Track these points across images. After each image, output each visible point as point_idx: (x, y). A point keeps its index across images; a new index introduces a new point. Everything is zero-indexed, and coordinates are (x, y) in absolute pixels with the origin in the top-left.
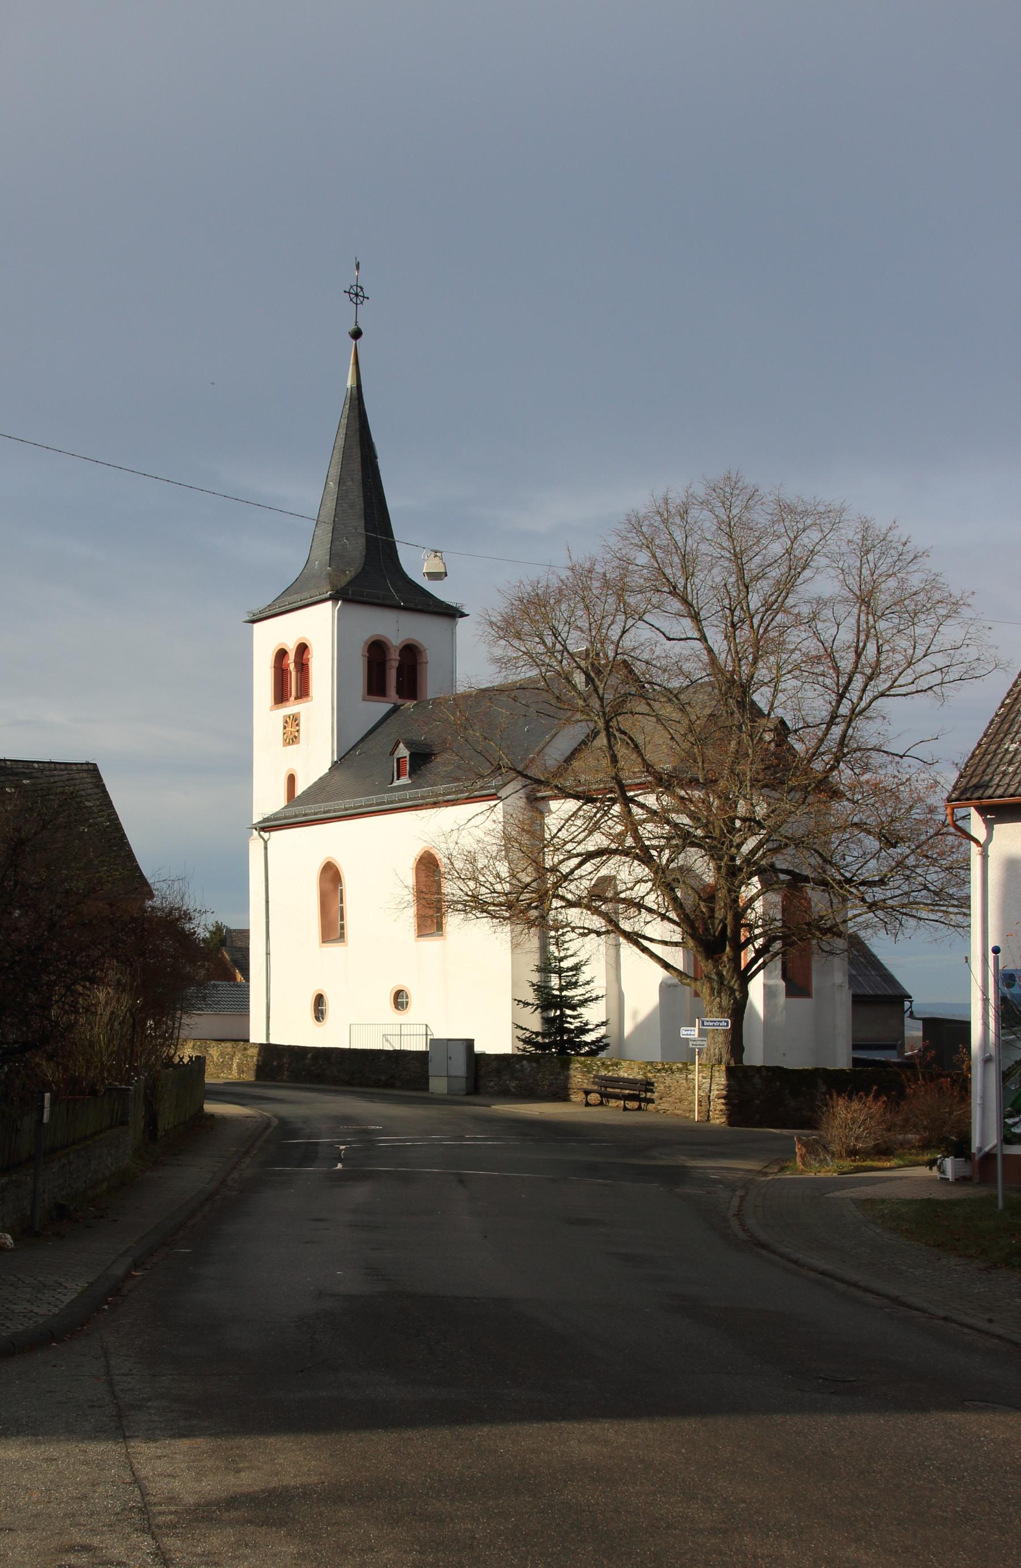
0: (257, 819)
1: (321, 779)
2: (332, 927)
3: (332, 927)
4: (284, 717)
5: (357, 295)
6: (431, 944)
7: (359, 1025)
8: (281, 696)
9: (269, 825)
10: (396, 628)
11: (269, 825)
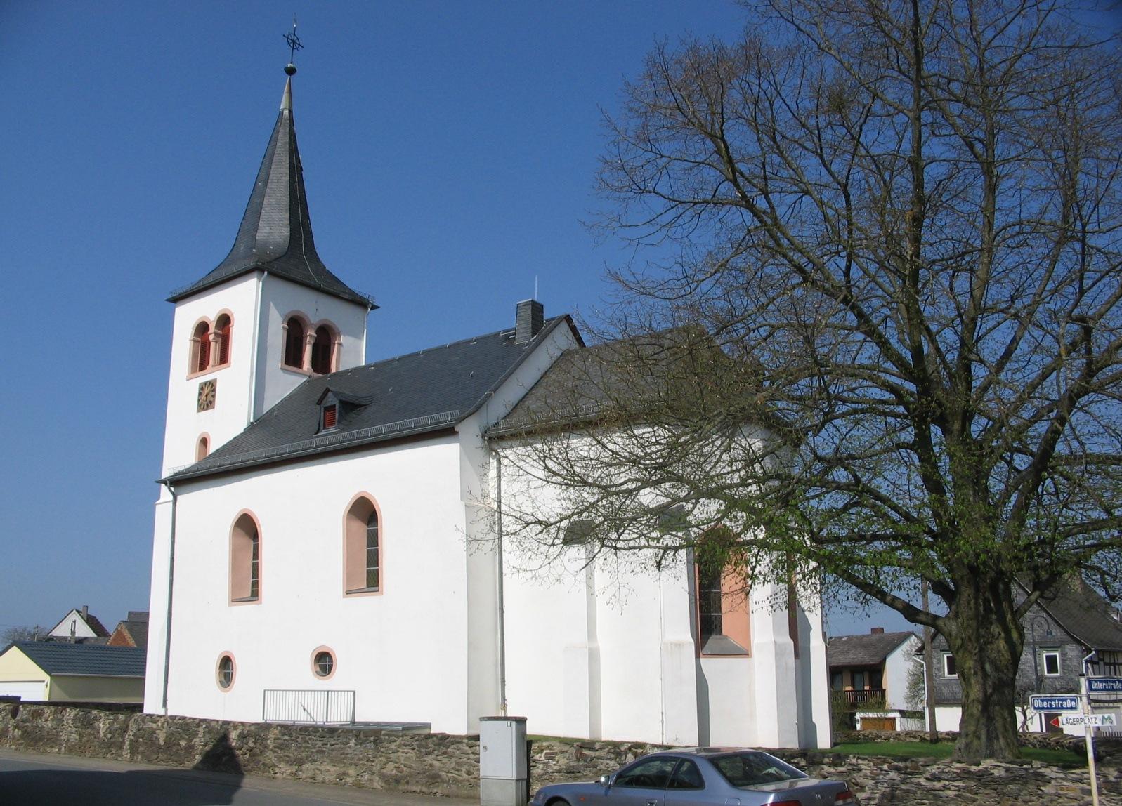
0: (166, 473)
1: (235, 438)
2: (248, 587)
3: (248, 587)
4: (200, 384)
5: (294, 42)
6: (366, 601)
7: (270, 693)
8: (201, 362)
9: (181, 481)
10: (316, 309)
11: (181, 481)
